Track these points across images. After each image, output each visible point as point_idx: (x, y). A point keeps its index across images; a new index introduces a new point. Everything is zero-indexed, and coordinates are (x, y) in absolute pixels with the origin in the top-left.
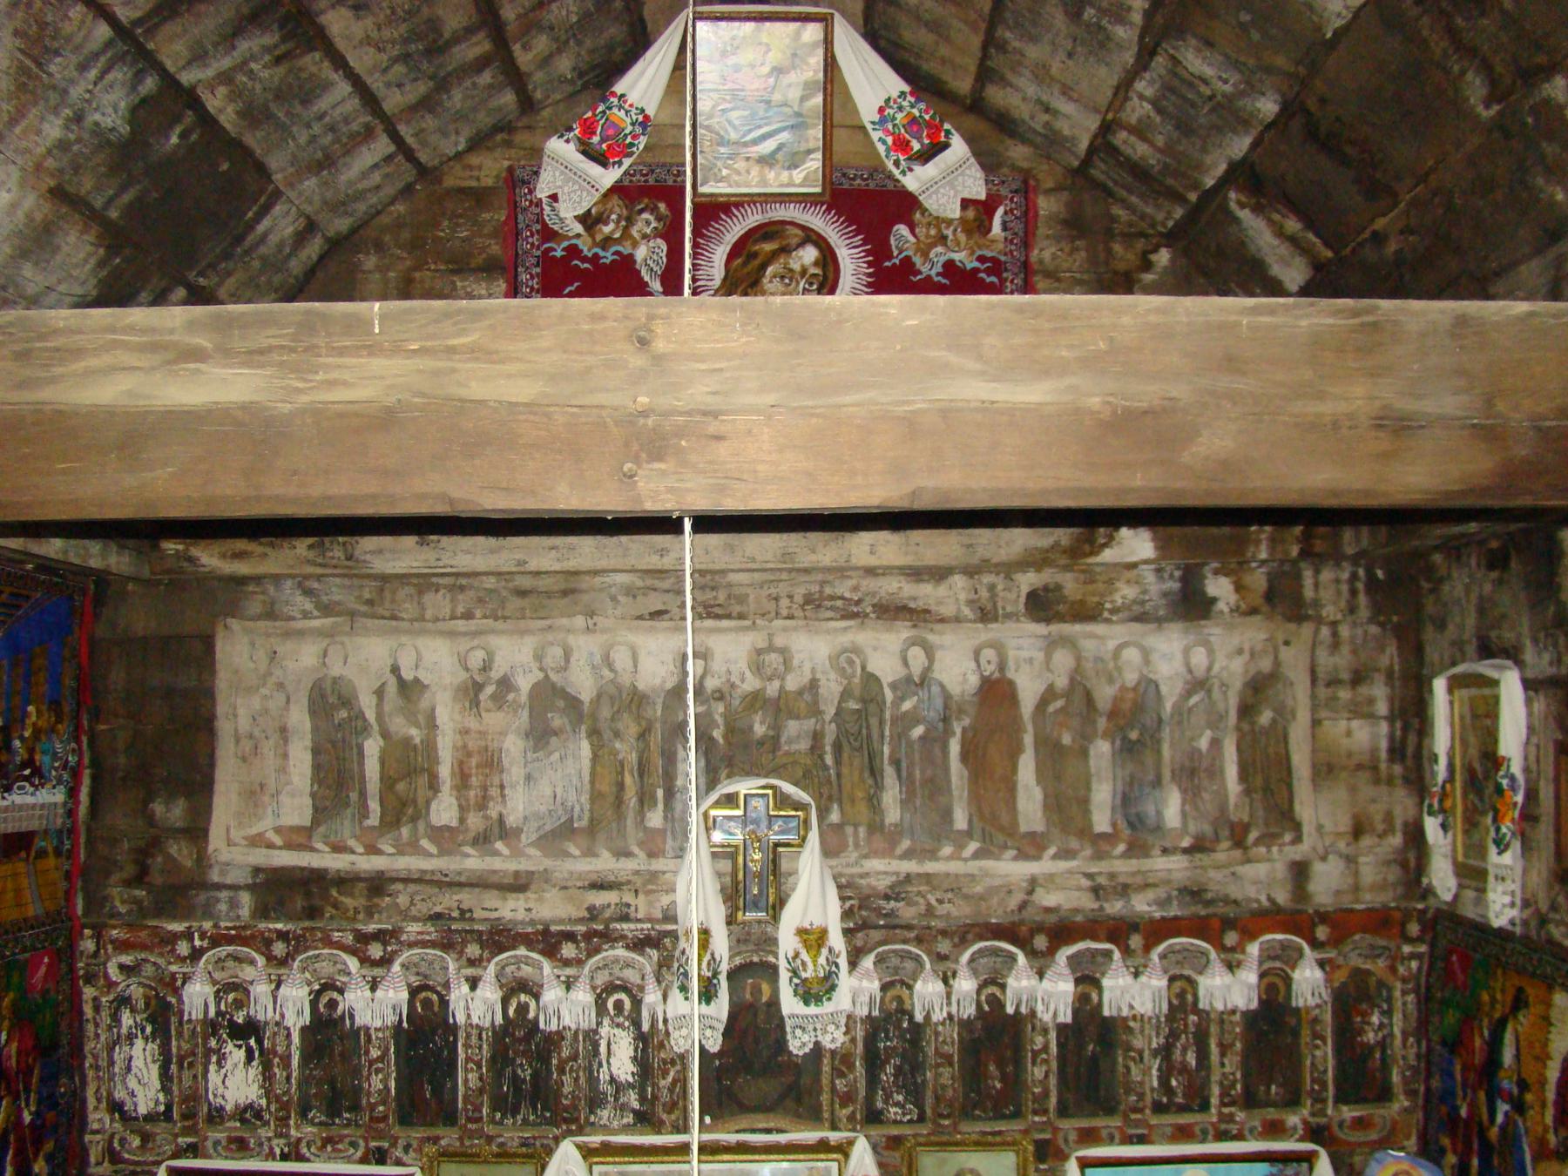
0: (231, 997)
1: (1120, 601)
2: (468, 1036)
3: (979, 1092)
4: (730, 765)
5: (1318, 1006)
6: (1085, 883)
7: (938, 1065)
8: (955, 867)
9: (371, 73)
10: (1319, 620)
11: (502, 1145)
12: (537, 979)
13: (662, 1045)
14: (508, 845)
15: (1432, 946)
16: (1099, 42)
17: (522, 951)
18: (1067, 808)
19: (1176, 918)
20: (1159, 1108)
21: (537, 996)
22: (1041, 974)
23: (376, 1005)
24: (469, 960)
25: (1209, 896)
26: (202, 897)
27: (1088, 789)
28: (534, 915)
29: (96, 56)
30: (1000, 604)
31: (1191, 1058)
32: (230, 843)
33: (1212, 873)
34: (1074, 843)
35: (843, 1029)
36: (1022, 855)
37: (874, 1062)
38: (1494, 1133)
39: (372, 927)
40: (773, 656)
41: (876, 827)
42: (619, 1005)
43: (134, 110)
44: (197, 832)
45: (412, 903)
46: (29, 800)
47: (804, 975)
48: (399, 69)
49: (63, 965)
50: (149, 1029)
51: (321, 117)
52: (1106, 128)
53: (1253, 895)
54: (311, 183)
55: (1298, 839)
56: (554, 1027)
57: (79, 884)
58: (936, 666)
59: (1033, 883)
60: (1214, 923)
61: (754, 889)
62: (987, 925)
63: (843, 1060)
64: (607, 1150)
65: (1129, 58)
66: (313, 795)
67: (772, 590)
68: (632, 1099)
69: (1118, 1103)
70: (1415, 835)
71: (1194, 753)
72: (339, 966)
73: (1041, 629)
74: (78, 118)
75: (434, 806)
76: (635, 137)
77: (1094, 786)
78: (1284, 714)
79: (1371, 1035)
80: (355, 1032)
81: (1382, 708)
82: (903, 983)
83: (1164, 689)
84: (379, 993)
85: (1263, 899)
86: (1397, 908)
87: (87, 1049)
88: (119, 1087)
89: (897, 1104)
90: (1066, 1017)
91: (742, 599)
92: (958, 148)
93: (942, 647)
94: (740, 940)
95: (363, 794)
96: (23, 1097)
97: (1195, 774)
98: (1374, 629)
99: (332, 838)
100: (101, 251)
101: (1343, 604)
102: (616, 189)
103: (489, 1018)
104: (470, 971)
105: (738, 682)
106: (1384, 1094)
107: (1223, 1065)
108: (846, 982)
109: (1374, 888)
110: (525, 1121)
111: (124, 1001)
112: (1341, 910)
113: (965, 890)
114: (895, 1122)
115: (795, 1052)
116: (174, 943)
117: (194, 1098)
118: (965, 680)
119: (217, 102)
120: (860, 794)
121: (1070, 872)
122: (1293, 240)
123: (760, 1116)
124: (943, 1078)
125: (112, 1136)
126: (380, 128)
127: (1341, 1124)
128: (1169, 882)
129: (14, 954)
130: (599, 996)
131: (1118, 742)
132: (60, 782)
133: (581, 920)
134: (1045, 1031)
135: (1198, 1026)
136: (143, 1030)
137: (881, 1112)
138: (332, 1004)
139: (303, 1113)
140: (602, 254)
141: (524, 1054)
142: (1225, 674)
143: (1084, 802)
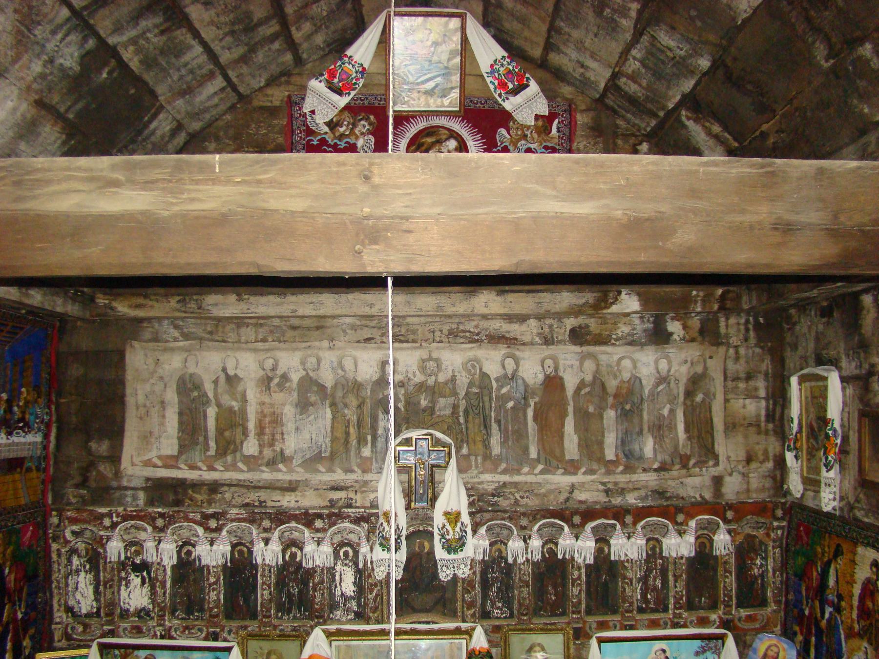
0: (133, 549)
1: (620, 334)
2: (264, 570)
3: (543, 603)
4: (408, 423)
5: (727, 554)
6: (601, 487)
7: (521, 587)
8: (530, 478)
9: (213, 41)
10: (728, 345)
11: (281, 630)
12: (301, 539)
13: (370, 576)
14: (286, 466)
15: (789, 522)
16: (613, 27)
17: (293, 524)
18: (591, 447)
19: (650, 507)
20: (641, 610)
21: (301, 549)
22: (577, 538)
23: (213, 554)
24: (264, 529)
25: (669, 494)
26: (117, 494)
27: (603, 436)
28: (299, 504)
29: (60, 27)
30: (555, 336)
31: (658, 583)
32: (133, 464)
33: (670, 482)
34: (595, 466)
35: (469, 567)
36: (566, 472)
37: (485, 584)
38: (824, 623)
39: (211, 511)
40: (431, 363)
41: (487, 457)
42: (346, 554)
43: (82, 57)
44: (115, 458)
45: (233, 498)
46: (22, 440)
47: (448, 537)
48: (229, 39)
49: (41, 531)
50: (88, 567)
51: (186, 65)
52: (615, 76)
53: (692, 494)
54: (180, 103)
55: (717, 464)
56: (311, 566)
57: (50, 487)
58: (520, 369)
59: (573, 487)
60: (670, 510)
61: (421, 491)
62: (548, 510)
63: (469, 584)
64: (339, 633)
65: (628, 36)
66: (179, 438)
67: (431, 327)
68: (353, 605)
69: (619, 607)
70: (780, 462)
71: (661, 417)
72: (193, 532)
73: (577, 349)
74: (51, 61)
75: (245, 444)
76: (357, 79)
77: (606, 434)
78: (709, 396)
79: (756, 570)
80: (201, 568)
81: (762, 393)
82: (502, 542)
83: (644, 382)
84: (215, 547)
85: (698, 496)
86: (770, 502)
87: (53, 578)
88: (71, 598)
89: (498, 608)
90: (590, 560)
91: (414, 332)
92: (534, 87)
93: (523, 359)
94: (413, 518)
95: (206, 438)
96: (18, 603)
97: (660, 428)
98: (758, 350)
99: (189, 462)
100: (64, 137)
101: (741, 336)
102: (347, 108)
103: (275, 561)
104: (265, 535)
105: (412, 377)
106: (764, 603)
107: (676, 587)
108: (471, 541)
109: (757, 490)
110: (295, 618)
111: (74, 551)
112: (740, 503)
113: (535, 491)
114: (497, 618)
115: (443, 579)
116: (102, 519)
117: (113, 604)
118: (536, 377)
119: (128, 55)
120: (478, 438)
121: (593, 481)
122: (716, 137)
123: (423, 615)
124: (523, 594)
125: (67, 626)
126: (218, 72)
127: (740, 619)
128: (647, 487)
129: (13, 525)
130: (335, 549)
131: (619, 411)
132: (39, 430)
133: (326, 507)
134: (579, 568)
135: (662, 565)
136: (85, 567)
137: (489, 612)
138: (189, 553)
139: (173, 612)
140: (339, 143)
141: (294, 580)
142: (677, 374)
143: (601, 444)
